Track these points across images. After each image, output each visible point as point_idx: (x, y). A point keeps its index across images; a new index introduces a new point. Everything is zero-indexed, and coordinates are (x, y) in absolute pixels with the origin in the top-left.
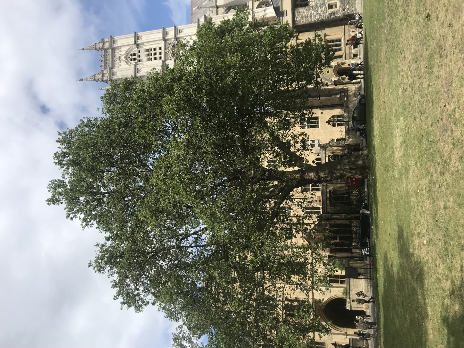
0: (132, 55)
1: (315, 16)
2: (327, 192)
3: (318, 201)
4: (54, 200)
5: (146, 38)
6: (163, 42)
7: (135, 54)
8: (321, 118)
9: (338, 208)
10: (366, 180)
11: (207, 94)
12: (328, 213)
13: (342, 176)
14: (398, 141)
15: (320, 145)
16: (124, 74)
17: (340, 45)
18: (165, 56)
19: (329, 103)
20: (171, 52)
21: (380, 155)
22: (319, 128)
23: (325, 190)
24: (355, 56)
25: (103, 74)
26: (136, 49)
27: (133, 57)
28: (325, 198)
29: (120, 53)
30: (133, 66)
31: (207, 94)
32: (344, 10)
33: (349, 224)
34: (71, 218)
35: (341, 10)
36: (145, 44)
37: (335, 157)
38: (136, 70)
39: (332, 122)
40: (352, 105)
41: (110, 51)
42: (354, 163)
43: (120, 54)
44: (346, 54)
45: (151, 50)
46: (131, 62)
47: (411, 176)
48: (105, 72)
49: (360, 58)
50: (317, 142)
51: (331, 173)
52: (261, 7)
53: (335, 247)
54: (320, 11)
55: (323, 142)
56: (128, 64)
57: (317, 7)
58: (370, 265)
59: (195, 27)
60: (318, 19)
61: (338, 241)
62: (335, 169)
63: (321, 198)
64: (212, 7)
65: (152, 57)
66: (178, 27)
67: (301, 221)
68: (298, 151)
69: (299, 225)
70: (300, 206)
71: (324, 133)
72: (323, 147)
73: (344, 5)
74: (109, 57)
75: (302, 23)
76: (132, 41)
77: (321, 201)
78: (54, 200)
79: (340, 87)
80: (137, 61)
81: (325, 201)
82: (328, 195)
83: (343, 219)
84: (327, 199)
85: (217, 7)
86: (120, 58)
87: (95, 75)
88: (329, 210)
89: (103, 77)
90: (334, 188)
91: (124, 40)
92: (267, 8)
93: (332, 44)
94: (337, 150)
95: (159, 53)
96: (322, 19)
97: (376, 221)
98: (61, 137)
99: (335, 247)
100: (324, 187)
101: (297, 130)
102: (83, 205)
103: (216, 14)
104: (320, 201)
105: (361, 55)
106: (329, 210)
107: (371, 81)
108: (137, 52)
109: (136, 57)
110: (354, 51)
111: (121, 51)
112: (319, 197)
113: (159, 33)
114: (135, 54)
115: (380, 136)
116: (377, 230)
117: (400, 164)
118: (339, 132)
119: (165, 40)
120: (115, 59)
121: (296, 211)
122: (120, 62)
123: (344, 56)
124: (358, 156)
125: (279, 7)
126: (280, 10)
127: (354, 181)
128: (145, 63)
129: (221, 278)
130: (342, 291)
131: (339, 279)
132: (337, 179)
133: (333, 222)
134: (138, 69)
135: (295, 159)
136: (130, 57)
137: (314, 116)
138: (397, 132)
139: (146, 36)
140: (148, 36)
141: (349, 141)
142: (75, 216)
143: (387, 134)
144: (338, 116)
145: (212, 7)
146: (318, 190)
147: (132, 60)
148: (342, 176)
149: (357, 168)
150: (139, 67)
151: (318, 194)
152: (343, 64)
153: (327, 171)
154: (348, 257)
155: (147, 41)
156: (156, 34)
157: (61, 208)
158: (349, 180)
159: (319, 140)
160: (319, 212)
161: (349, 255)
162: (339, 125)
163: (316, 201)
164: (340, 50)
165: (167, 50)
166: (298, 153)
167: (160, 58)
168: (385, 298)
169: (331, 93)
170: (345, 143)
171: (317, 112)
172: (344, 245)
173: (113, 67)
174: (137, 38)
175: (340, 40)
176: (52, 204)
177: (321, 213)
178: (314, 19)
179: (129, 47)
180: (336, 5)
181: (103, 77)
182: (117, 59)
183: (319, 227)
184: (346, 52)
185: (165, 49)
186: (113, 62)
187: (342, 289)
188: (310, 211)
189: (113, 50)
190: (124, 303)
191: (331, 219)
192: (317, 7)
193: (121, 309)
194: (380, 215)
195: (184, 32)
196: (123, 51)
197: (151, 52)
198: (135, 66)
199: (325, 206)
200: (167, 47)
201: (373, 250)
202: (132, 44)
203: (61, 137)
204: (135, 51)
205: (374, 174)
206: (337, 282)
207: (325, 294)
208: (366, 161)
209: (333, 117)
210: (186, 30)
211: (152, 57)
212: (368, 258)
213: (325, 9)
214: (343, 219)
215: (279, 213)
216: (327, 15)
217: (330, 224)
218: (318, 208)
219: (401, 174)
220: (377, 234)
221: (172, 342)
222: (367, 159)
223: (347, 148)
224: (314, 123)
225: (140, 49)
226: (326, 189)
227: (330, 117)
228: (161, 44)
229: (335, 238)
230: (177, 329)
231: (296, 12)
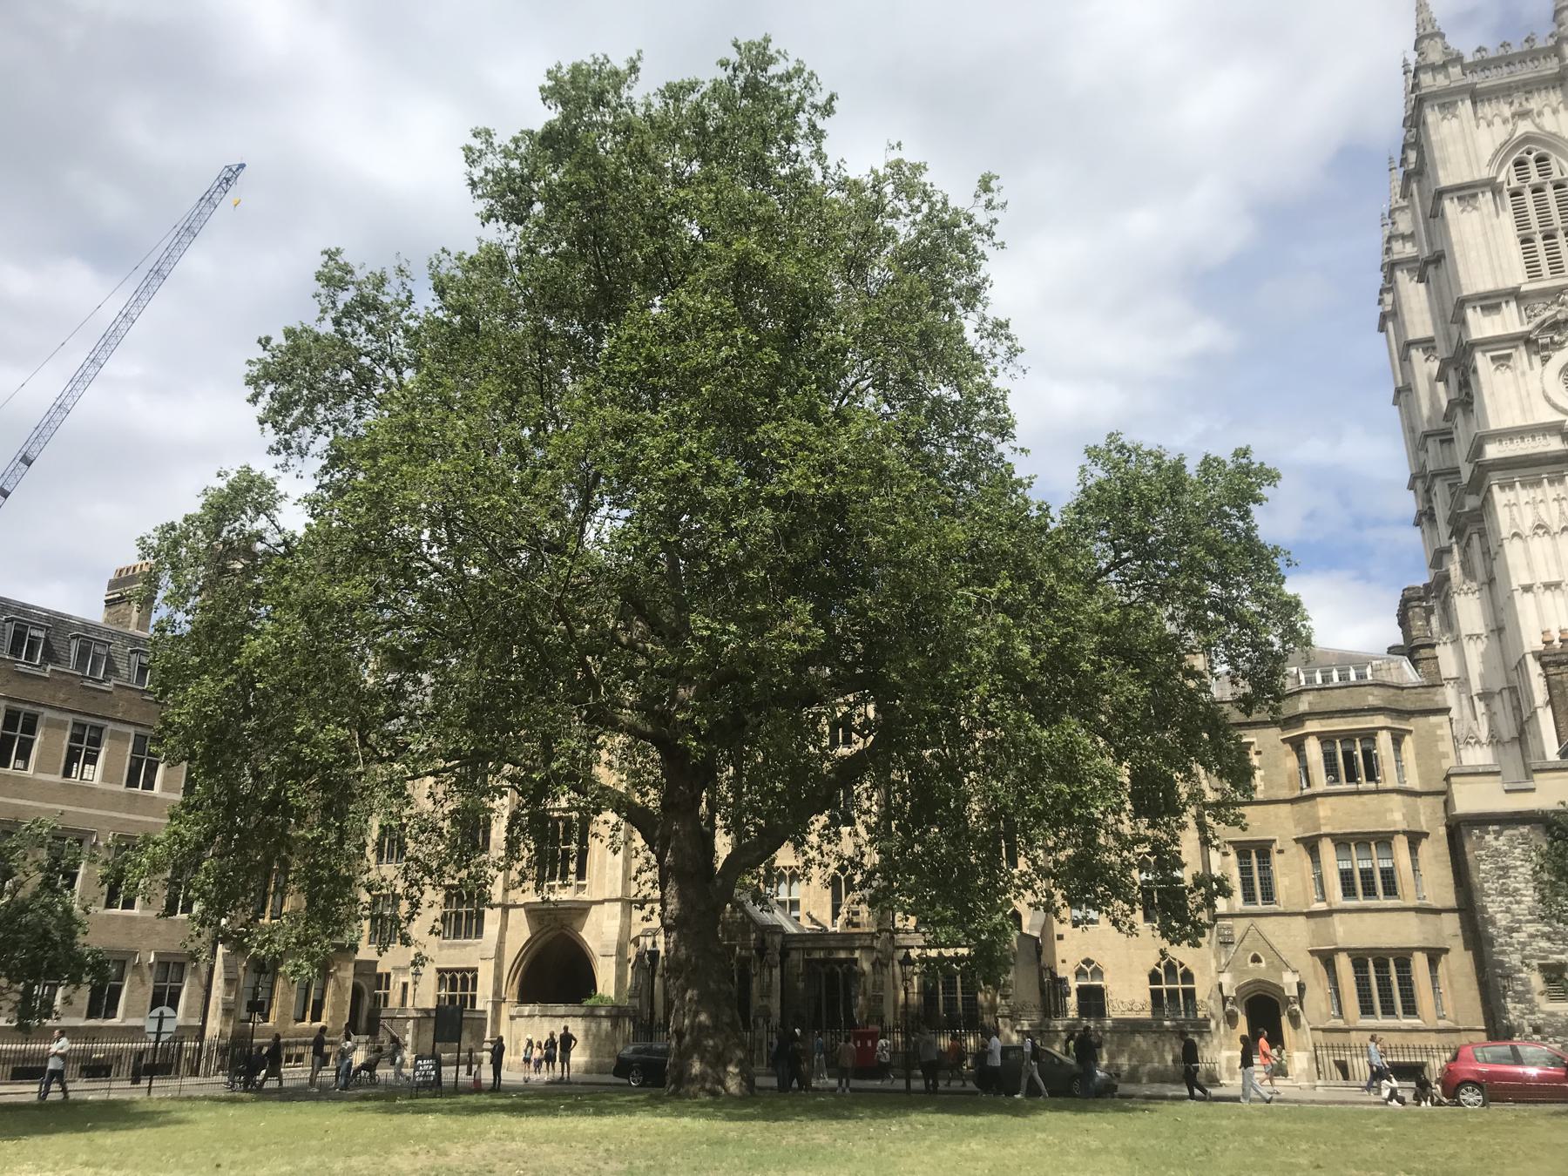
0: (1541, 159)
1: (1508, 910)
2: (852, 950)
7: (1544, 173)
9: (801, 985)
12: (785, 953)
16: (1451, 149)
17: (1388, 1010)
18: (1543, 294)
23: (857, 944)
25: (1444, 66)
27: (1532, 166)
28: (833, 944)
29: (1547, 111)
30: (1485, 173)
32: (1537, 1030)
35: (1538, 1019)
38: (1467, 192)
40: (1144, 1046)
42: (697, 1046)
43: (1540, 114)
44: (1347, 1031)
46: (1510, 163)
48: (1455, 71)
56: (1497, 152)
62: (687, 979)
65: (1539, 243)
74: (1525, 72)
80: (1515, 184)
81: (822, 944)
82: (843, 955)
84: (830, 950)
86: (1524, 115)
87: (1442, 36)
88: (795, 956)
90: (864, 973)
97: (546, 1106)
100: (868, 942)
108: (1556, 176)
109: (1535, 178)
111: (1555, 111)
114: (1544, 173)
120: (1518, 98)
122: (1505, 121)
123: (1340, 1023)
128: (1507, 220)
134: (1475, 196)
141: (1007, 1031)
147: (1520, 163)
162: (1156, 995)
164: (1367, 1009)
167: (1533, 269)
170: (1003, 1016)
173: (1477, 97)
184: (1353, 1034)
186: (1504, 92)
198: (1493, 186)
199: (809, 945)
211: (1539, 243)
213: (1541, 950)
217: (747, 960)
226: (862, 948)
227: (1188, 965)
231: (1525, 830)
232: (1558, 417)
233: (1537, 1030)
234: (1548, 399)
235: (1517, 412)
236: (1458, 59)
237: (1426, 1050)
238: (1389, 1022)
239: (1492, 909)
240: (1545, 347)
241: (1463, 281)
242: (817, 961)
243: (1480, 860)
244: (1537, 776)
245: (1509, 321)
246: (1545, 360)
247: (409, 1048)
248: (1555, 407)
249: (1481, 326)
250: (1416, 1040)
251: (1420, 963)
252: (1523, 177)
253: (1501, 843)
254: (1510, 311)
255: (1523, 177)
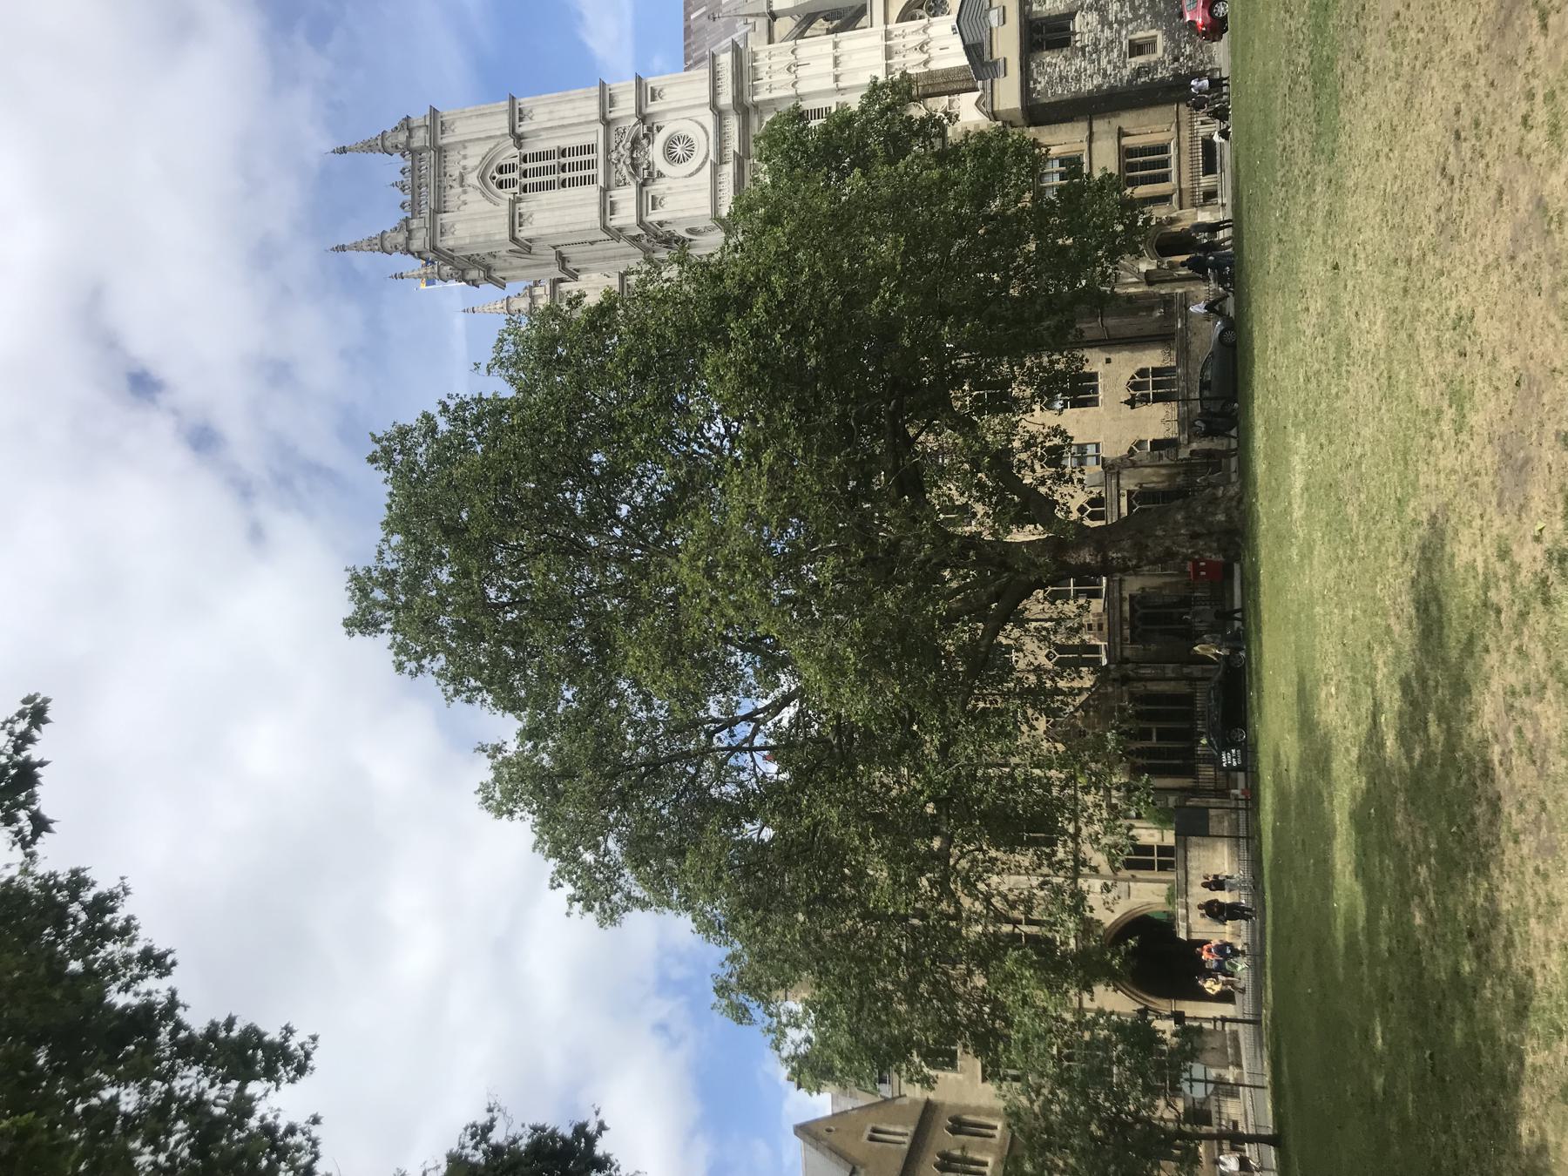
0: (500, 170)
1: (1091, 76)
2: (1122, 599)
3: (1095, 627)
4: (361, 623)
5: (546, 117)
6: (601, 128)
7: (512, 168)
8: (1105, 376)
9: (1153, 647)
10: (1237, 567)
11: (817, 347)
13: (1169, 555)
14: (1298, 482)
15: (1103, 462)
16: (479, 230)
17: (1165, 164)
18: (607, 173)
19: (1128, 333)
20: (628, 161)
21: (1266, 503)
22: (1101, 408)
24: (1210, 195)
25: (410, 231)
26: (515, 151)
30: (505, 206)
31: (817, 347)
32: (1176, 59)
33: (1185, 700)
34: (411, 672)
36: (544, 135)
37: (1141, 496)
38: (515, 220)
39: (1143, 390)
41: (429, 156)
43: (464, 168)
45: (563, 153)
46: (500, 191)
47: (1315, 562)
48: (415, 224)
49: (1223, 205)
50: (1091, 450)
51: (1140, 548)
52: (913, 18)
53: (1145, 762)
54: (1104, 62)
55: (1107, 453)
56: (488, 199)
57: (1096, 51)
58: (1246, 800)
59: (702, 80)
60: (1099, 87)
61: (1153, 742)
63: (1105, 617)
64: (757, 15)
66: (650, 80)
67: (1049, 684)
68: (1043, 483)
69: (1039, 697)
70: (1045, 639)
71: (1113, 422)
72: (1112, 469)
73: (1178, 46)
75: (1049, 98)
76: (501, 124)
77: (1105, 627)
78: (361, 623)
79: (1164, 290)
82: (1126, 607)
83: (1171, 679)
85: (773, 16)
89: (409, 238)
91: (474, 120)
92: (933, 20)
93: (1141, 159)
94: (1153, 478)
95: (590, 165)
96: (1112, 87)
98: (377, 447)
99: (1145, 762)
101: (1038, 420)
102: (452, 638)
103: (766, 38)
104: (1100, 627)
105: (1226, 198)
106: (1127, 653)
107: (1250, 305)
108: (516, 161)
109: (516, 175)
110: (1206, 182)
111: (465, 157)
112: (1099, 615)
113: (587, 98)
114: (512, 168)
115: (1266, 456)
116: (1259, 698)
117: (1301, 534)
118: (1158, 421)
119: (607, 123)
120: (447, 181)
121: (1030, 655)
122: (465, 192)
123: (1175, 197)
124: (1214, 500)
125: (981, 45)
126: (987, 57)
127: (1203, 569)
128: (545, 196)
129: (846, 824)
130: (1165, 893)
131: (1155, 858)
132: (1153, 563)
133: (1139, 687)
135: (1037, 507)
136: (498, 177)
137: (1087, 369)
138: (1296, 460)
139: (547, 110)
140: (551, 107)
142: (420, 668)
143: (1279, 457)
144: (1157, 372)
145: (757, 15)
146: (1095, 594)
147: (500, 185)
148: (1169, 555)
149: (1210, 534)
150: (523, 207)
151: (1097, 605)
152: (1172, 221)
153: (1126, 544)
154: (1182, 790)
155: (549, 124)
156: (577, 104)
157: (377, 649)
158: (1189, 564)
159: (1097, 445)
160: (1099, 660)
161: (1186, 782)
162: (1158, 399)
163: (1090, 627)
164: (1165, 178)
165: (614, 155)
166: (1043, 490)
167: (590, 180)
168: (1276, 867)
169: (1132, 304)
171: (1095, 361)
172: (1172, 754)
173: (439, 209)
174: (517, 115)
175: (1164, 149)
176: (358, 635)
177: (1105, 662)
178: (1088, 86)
179: (491, 144)
180: (1154, 43)
181: (409, 238)
182: (456, 184)
183: (1097, 703)
185: (608, 151)
186: (440, 190)
187: (1165, 886)
188: (1072, 658)
189: (441, 151)
190: (572, 899)
191: (1134, 680)
192: (1096, 51)
193: (568, 914)
194: (1267, 656)
195: (667, 98)
196: (474, 157)
197: (563, 160)
198: (514, 202)
200: (613, 146)
201: (1249, 751)
202: (503, 135)
203: (377, 447)
204: (509, 154)
205: (1254, 552)
206: (1148, 866)
207: (1116, 899)
208: (1236, 513)
209: (1142, 373)
210: (675, 89)
211: (567, 175)
212: (1241, 775)
214: (1171, 679)
215: (987, 662)
216: (1126, 73)
218: (1096, 649)
219: (1302, 557)
220: (1260, 707)
221: (714, 998)
222: (1237, 508)
223: (1181, 470)
224: (1081, 391)
225: (526, 151)
227: (1133, 372)
228: (595, 135)
229: (1145, 734)
230: (722, 965)
231: (1033, 65)
232: (708, 165)
233: (1176, 59)
234: (691, 175)
235: (699, 195)
236: (407, 220)
237: (1192, 139)
238: (1173, 162)
239: (1090, 86)
240: (650, 174)
241: (588, 226)
242: (1132, 633)
243: (1054, 94)
244: (995, 56)
245: (626, 197)
246: (661, 175)
247: (1222, 1072)
248: (698, 170)
249: (626, 215)
250: (1185, 145)
251: (1125, 141)
252: (514, 182)
253: (1043, 81)
254: (617, 194)
255: (514, 182)
